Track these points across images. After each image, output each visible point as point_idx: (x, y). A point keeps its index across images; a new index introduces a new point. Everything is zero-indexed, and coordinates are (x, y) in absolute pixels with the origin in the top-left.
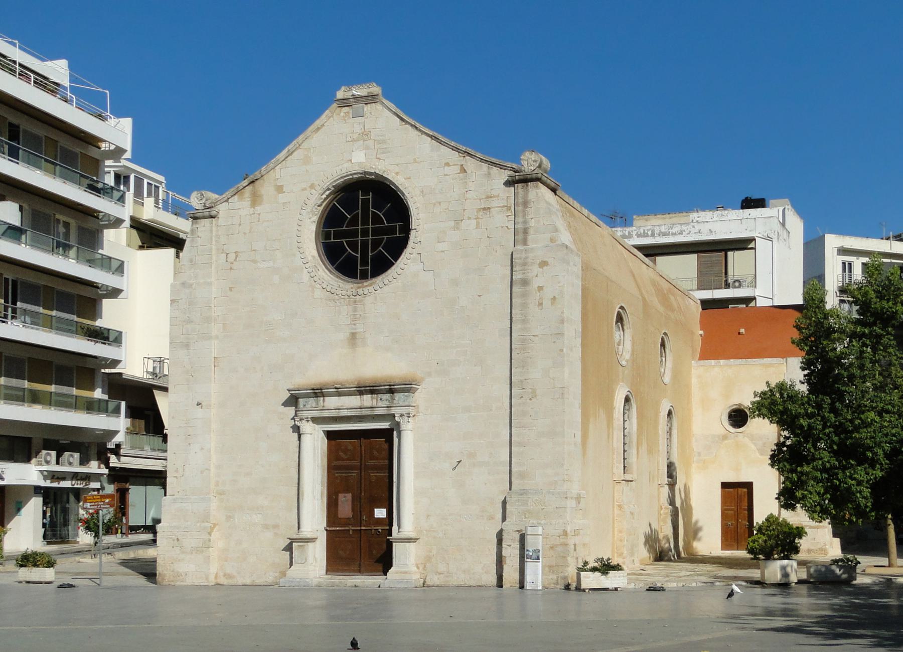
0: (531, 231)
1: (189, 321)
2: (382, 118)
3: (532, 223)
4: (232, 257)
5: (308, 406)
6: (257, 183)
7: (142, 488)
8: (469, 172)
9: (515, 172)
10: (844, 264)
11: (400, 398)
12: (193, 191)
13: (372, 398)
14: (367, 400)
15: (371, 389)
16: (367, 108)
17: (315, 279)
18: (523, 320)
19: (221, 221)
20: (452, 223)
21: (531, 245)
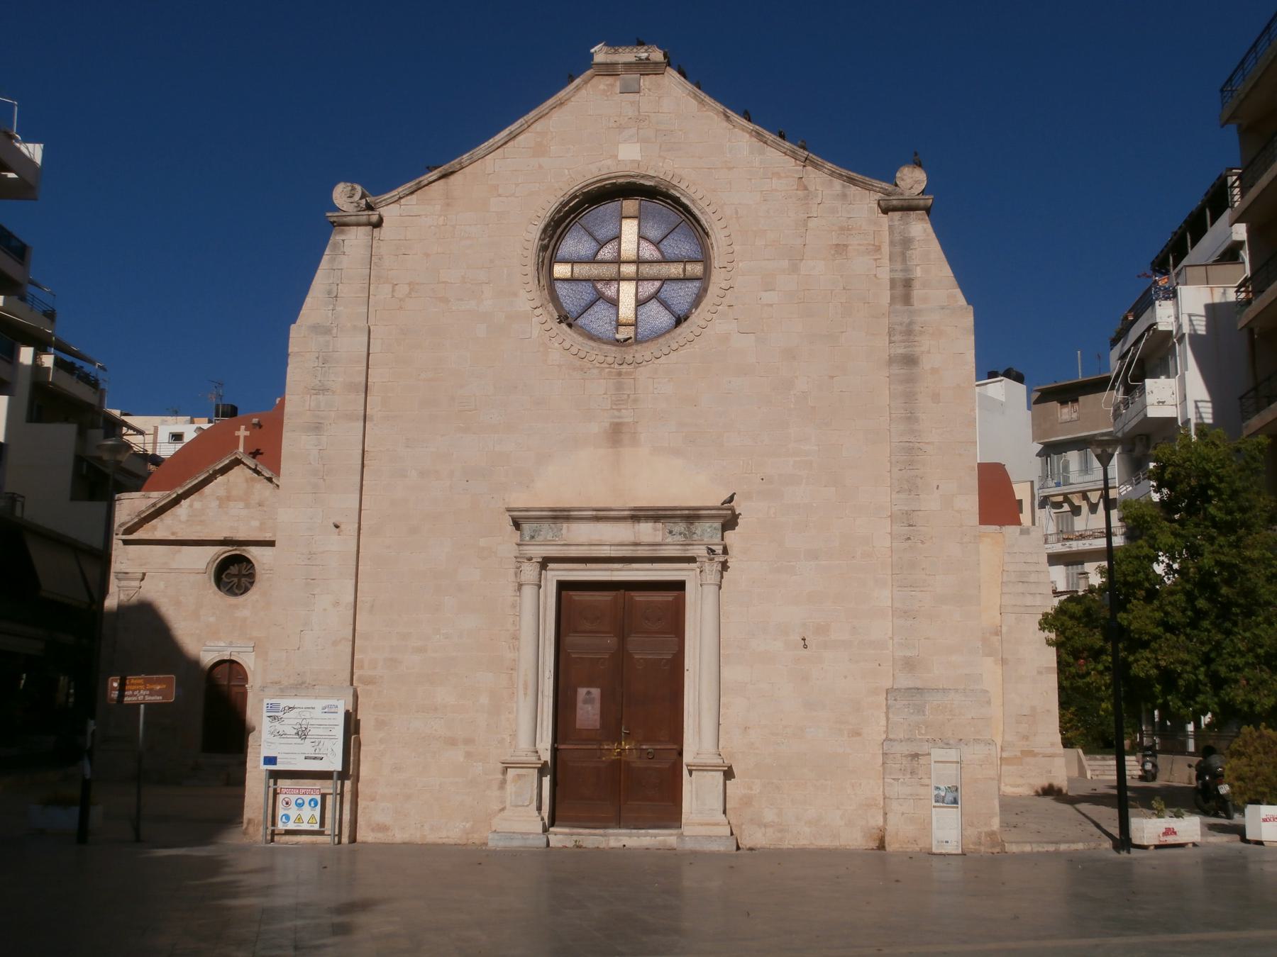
0: (916, 284)
1: (323, 390)
2: (672, 94)
3: (918, 272)
4: (403, 290)
5: (539, 539)
6: (452, 178)
7: (1014, 486)
8: (812, 188)
9: (888, 195)
10: (126, 542)
11: (703, 531)
12: (339, 182)
13: (655, 529)
14: (647, 531)
15: (656, 515)
16: (646, 82)
17: (552, 333)
18: (909, 418)
19: (386, 230)
20: (785, 264)
21: (917, 304)
